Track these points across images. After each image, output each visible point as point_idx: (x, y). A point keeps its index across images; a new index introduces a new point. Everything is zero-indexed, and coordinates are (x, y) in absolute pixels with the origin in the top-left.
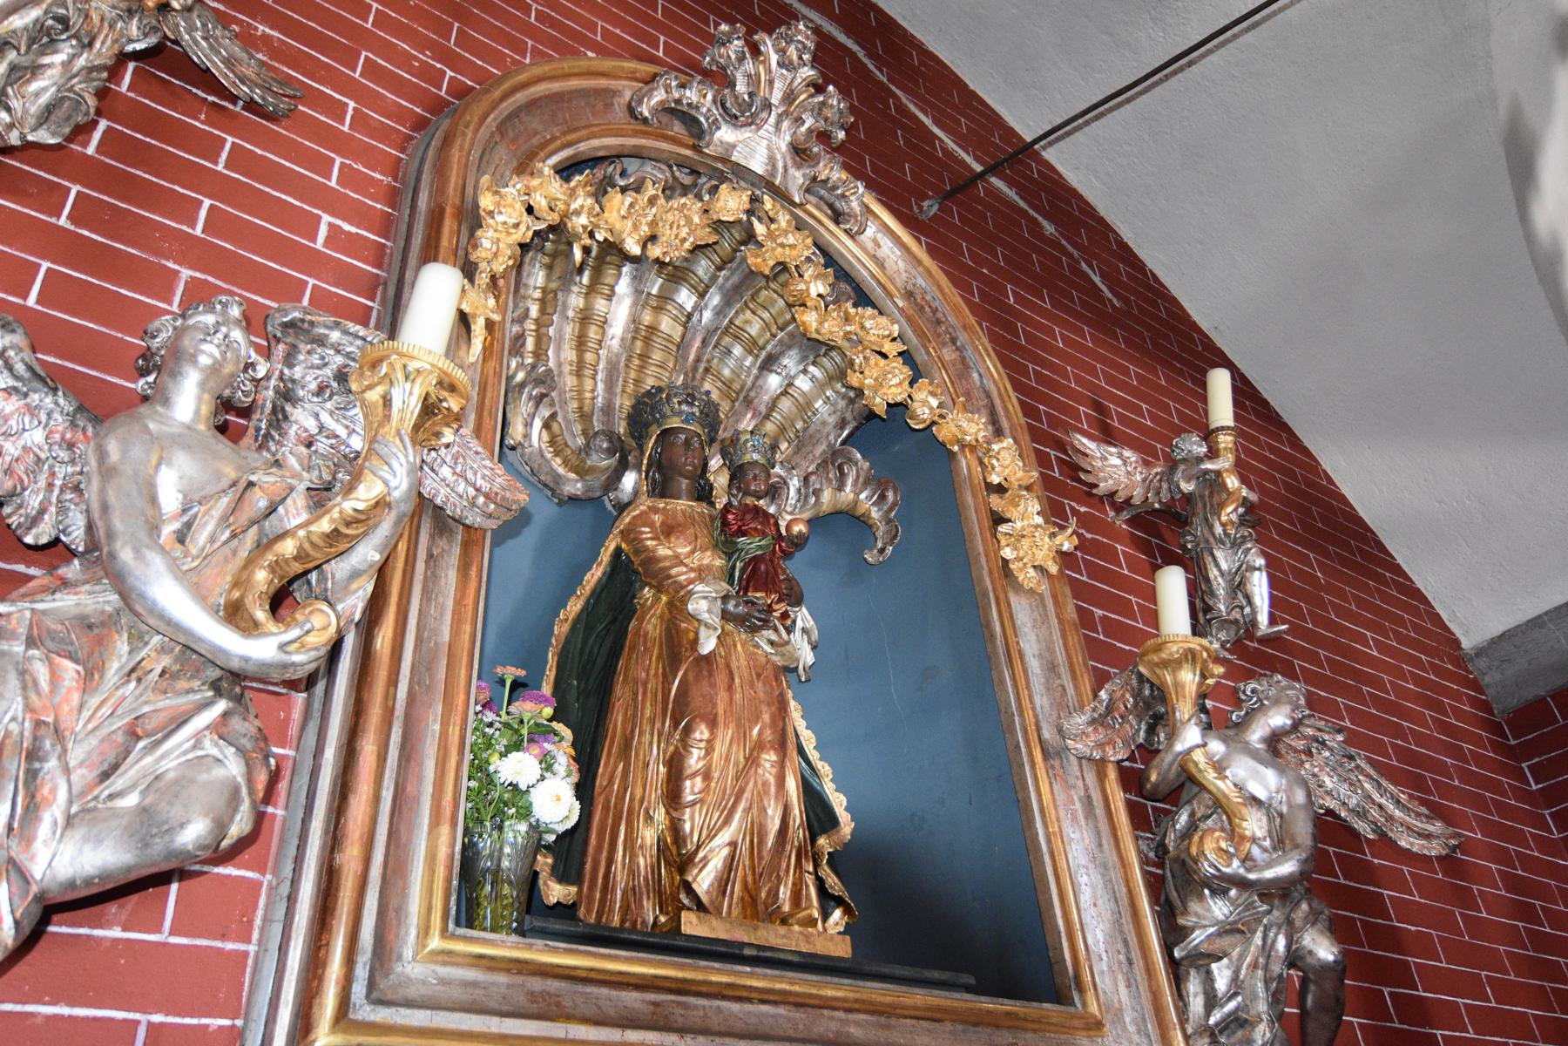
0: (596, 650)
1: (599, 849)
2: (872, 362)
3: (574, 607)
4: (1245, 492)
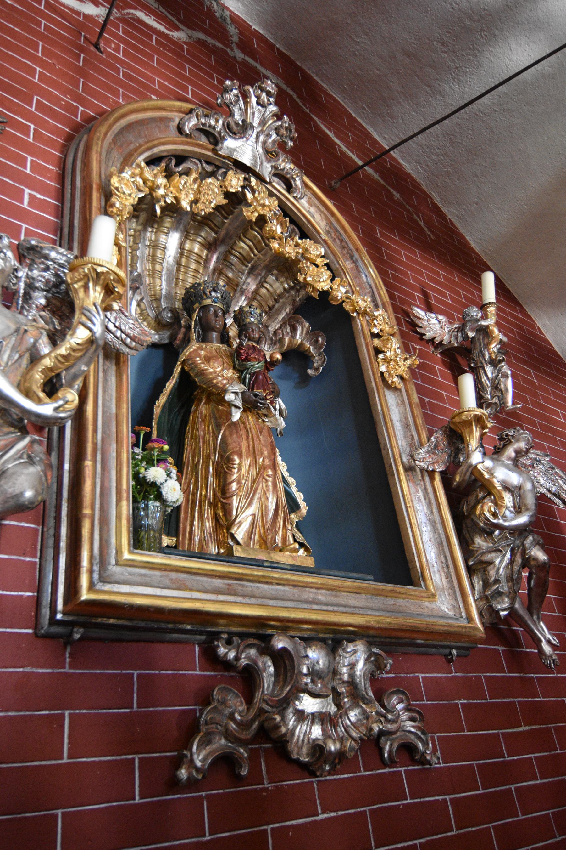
0: (174, 422)
1: (186, 519)
2: (311, 269)
3: (162, 399)
4: (501, 337)
